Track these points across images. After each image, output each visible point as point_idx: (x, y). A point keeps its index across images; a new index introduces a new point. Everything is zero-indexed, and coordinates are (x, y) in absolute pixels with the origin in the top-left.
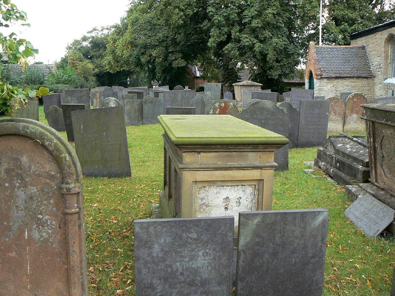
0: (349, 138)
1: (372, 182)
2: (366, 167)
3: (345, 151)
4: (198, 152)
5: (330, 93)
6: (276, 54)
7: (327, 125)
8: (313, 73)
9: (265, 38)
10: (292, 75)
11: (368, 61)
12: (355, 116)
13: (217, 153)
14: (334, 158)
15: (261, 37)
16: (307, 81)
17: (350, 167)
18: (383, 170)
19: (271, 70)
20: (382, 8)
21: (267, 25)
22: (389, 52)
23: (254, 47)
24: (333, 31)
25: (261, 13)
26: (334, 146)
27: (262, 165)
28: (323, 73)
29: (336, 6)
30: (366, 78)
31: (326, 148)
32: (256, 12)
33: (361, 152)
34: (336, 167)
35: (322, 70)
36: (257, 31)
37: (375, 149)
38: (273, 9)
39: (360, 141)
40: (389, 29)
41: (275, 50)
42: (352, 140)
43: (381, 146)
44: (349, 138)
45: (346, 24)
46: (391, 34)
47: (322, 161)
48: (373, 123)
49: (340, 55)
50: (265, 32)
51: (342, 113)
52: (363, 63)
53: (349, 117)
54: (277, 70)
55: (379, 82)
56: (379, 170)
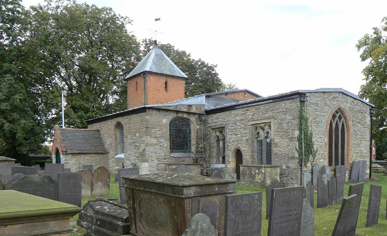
0: (105, 201)
1: (133, 233)
2: (124, 223)
3: (104, 211)
4: (5, 225)
5: (74, 166)
6: (24, 134)
7: (81, 192)
8: (60, 150)
9: (14, 119)
10: (39, 150)
11: (102, 141)
12: (100, 183)
13: (23, 225)
14: (94, 218)
15: (10, 118)
16: (54, 156)
17: (110, 223)
18: (142, 223)
19: (20, 146)
20: (107, 101)
21: (15, 109)
22: (118, 135)
23: (3, 127)
24: (73, 117)
25: (9, 98)
26: (93, 209)
27: (61, 230)
28: (68, 150)
29: (74, 97)
30: (102, 154)
31: (86, 210)
32: (4, 97)
33: (118, 211)
34: (97, 225)
35: (67, 147)
36: (5, 112)
37: (134, 209)
38: (20, 96)
39: (116, 203)
40: (116, 119)
41: (23, 130)
42: (108, 202)
43: (140, 206)
44: (105, 201)
45: (83, 112)
46: (118, 122)
47: (84, 221)
48: (132, 189)
49: (81, 136)
50: (13, 114)
51: (90, 182)
52: (98, 143)
53: (96, 185)
54: (26, 146)
55: (112, 157)
56: (139, 224)
